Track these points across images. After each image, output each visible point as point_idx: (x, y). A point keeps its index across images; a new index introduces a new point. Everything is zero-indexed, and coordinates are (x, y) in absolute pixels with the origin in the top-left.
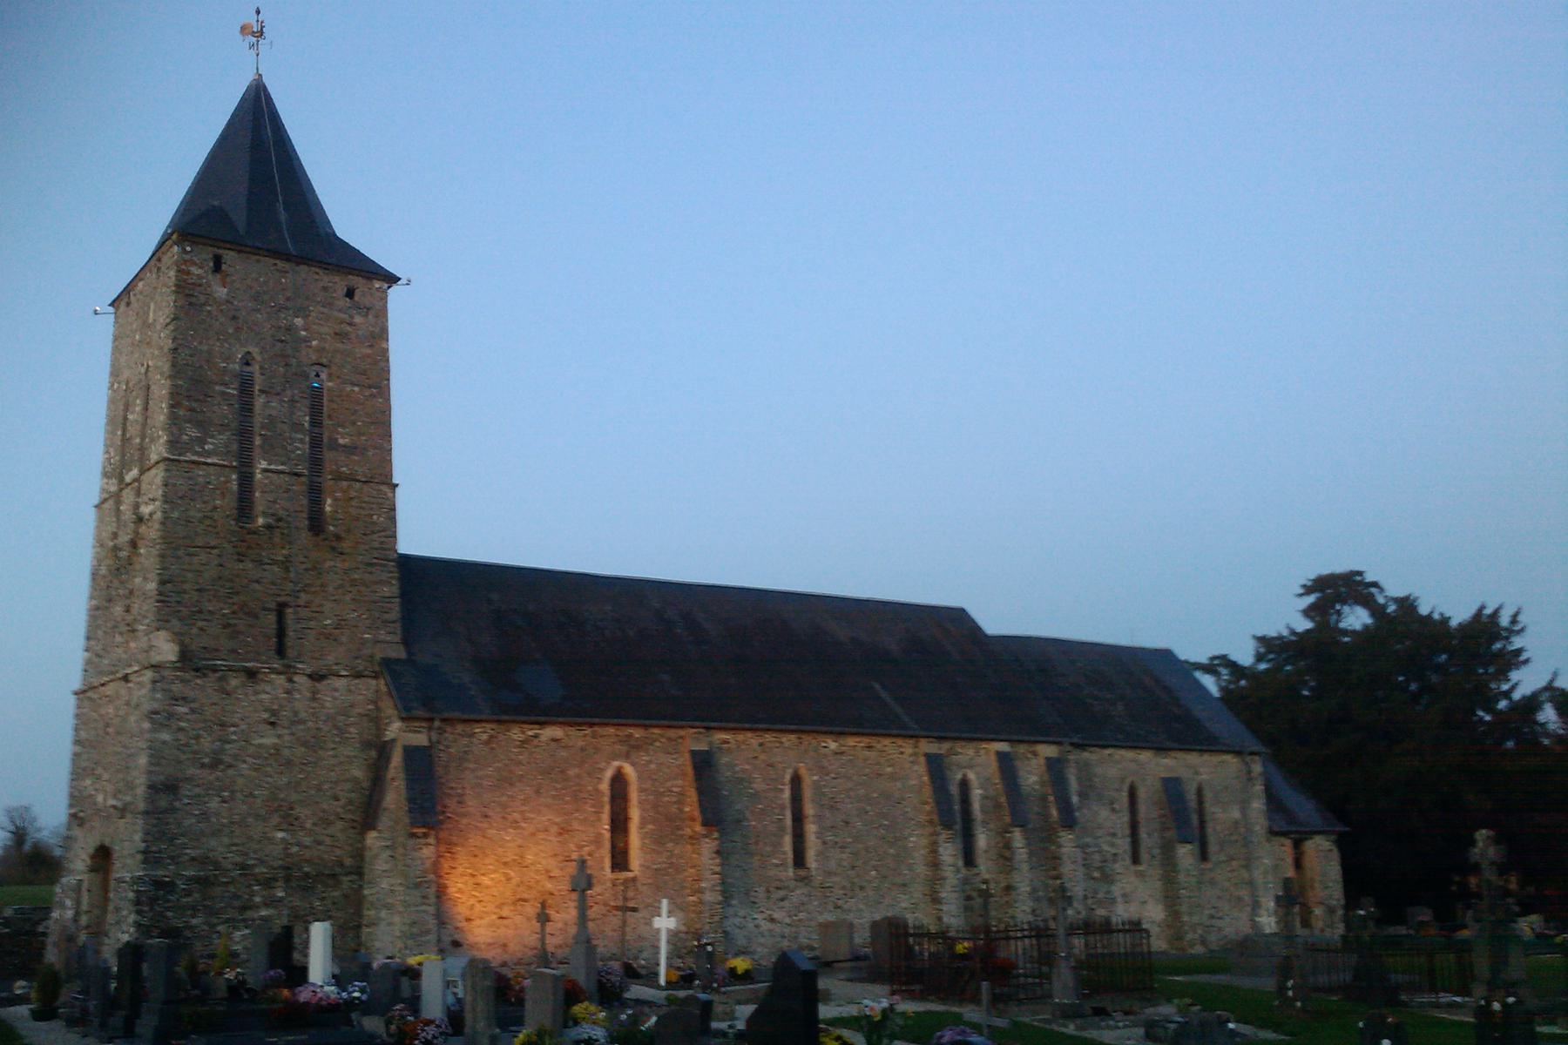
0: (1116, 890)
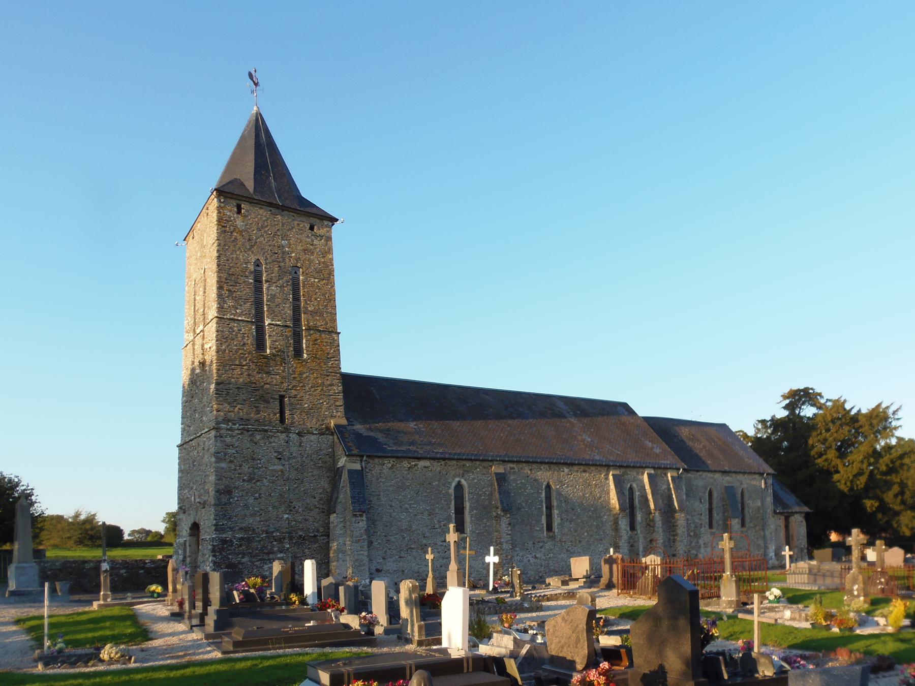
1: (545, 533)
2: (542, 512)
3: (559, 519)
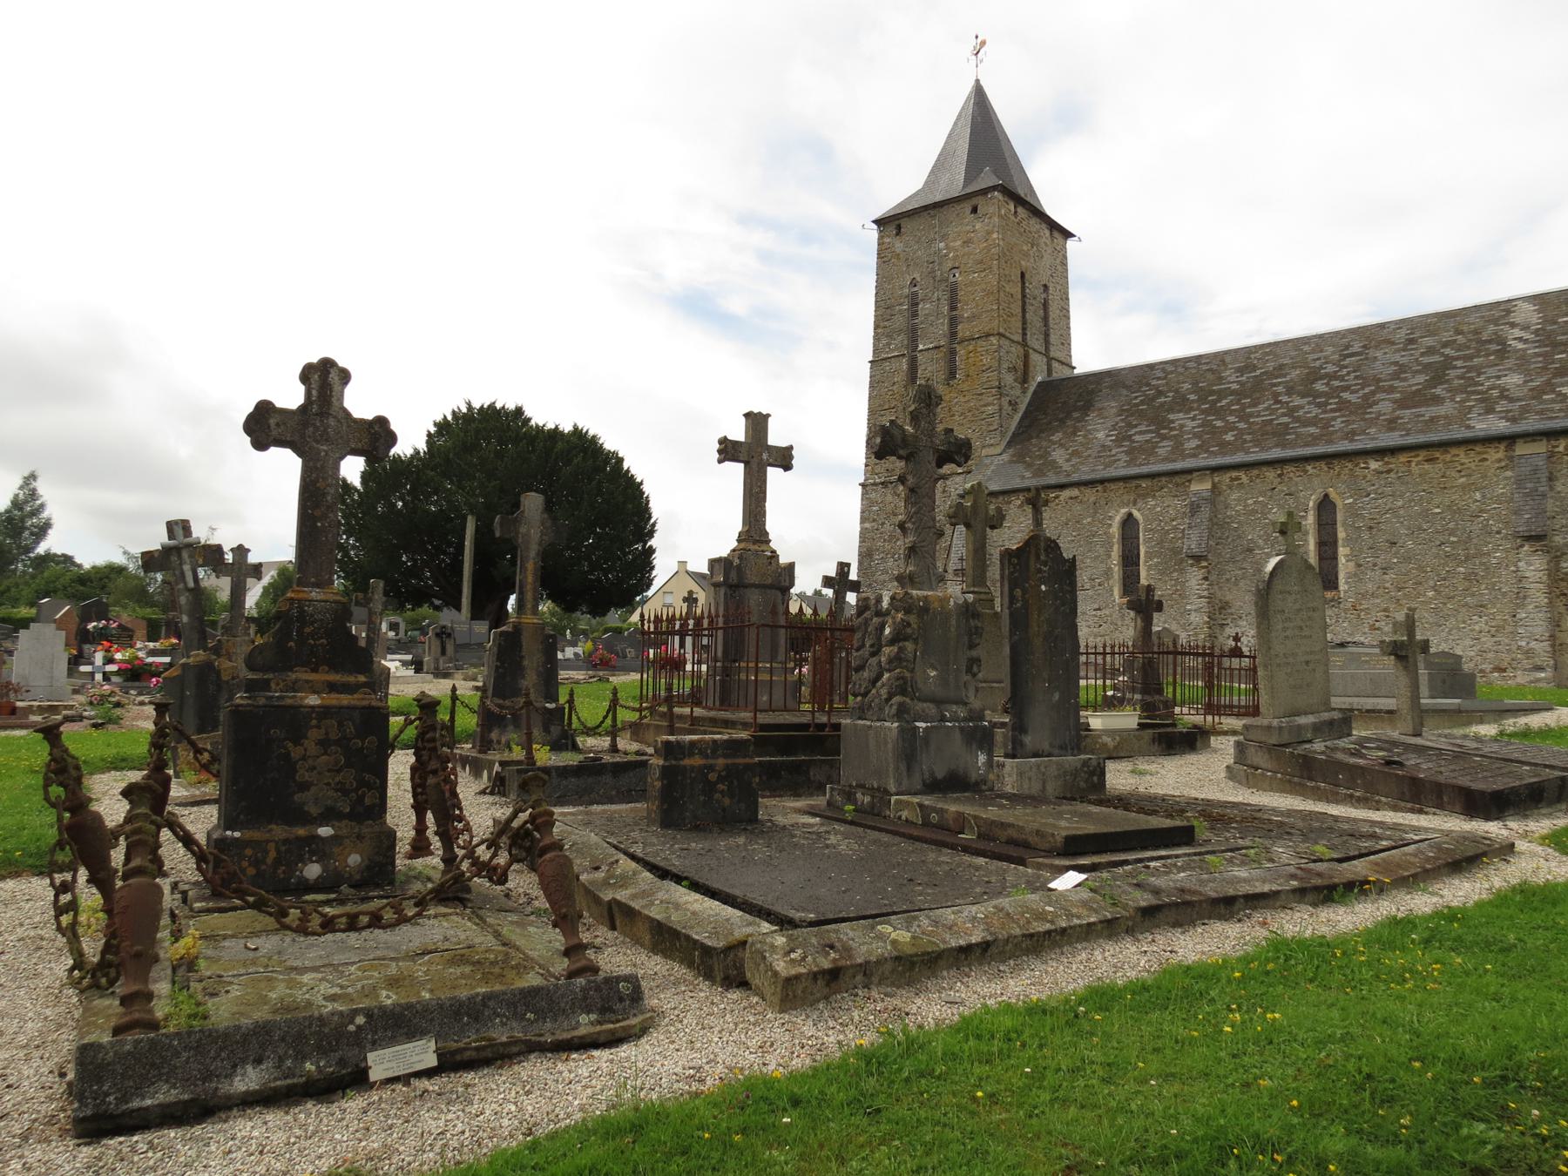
3: (1351, 564)
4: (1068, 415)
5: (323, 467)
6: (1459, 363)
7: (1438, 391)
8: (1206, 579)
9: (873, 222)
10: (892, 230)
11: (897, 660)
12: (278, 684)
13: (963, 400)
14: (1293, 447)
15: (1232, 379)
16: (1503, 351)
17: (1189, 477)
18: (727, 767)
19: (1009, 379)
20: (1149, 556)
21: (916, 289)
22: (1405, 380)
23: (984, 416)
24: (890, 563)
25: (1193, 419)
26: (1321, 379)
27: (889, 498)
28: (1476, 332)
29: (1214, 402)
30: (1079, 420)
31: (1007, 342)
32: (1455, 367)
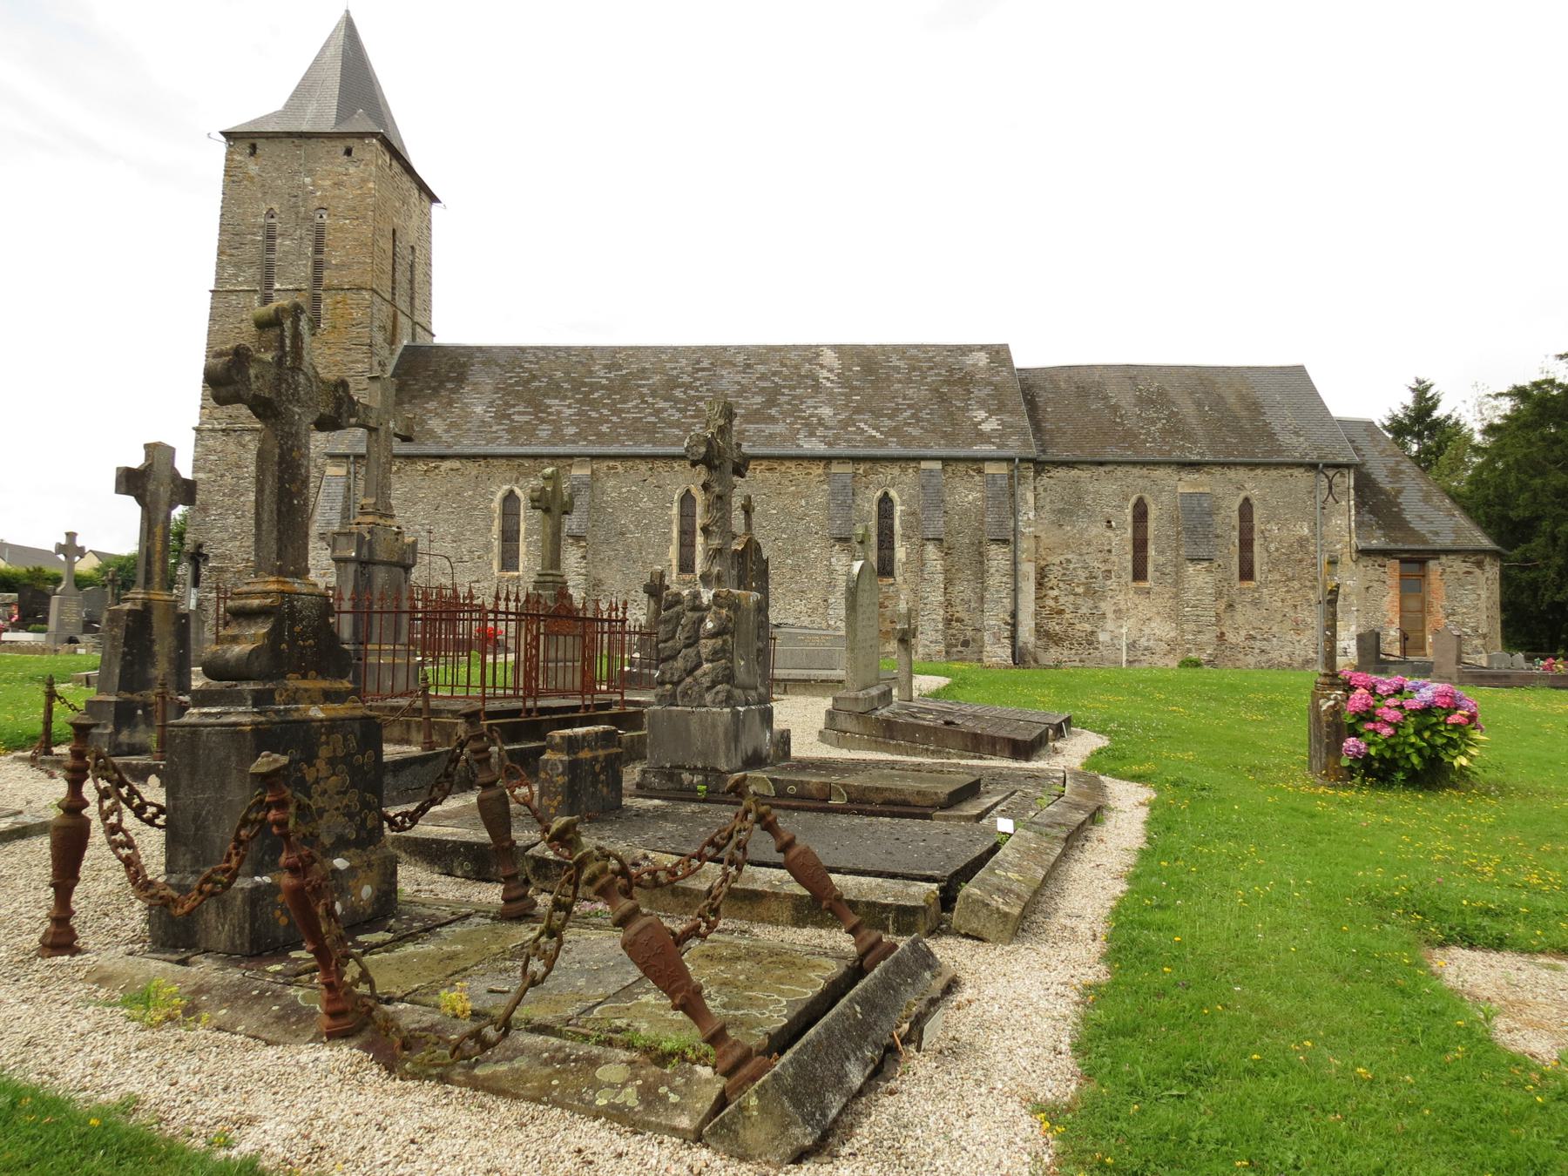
0: (1106, 606)
1: (674, 575)
2: (670, 540)
4: (442, 384)
5: (297, 433)
6: (786, 391)
7: (773, 411)
8: (584, 557)
9: (222, 133)
10: (244, 147)
11: (715, 655)
12: (281, 695)
13: (327, 352)
14: (662, 445)
15: (602, 376)
16: (817, 387)
17: (570, 462)
18: (607, 756)
19: (379, 338)
20: (529, 533)
21: (273, 221)
22: (746, 398)
23: (352, 373)
24: (231, 520)
25: (569, 406)
26: (679, 386)
27: (232, 447)
28: (797, 367)
29: (586, 394)
30: (453, 391)
31: (379, 300)
32: (783, 394)
